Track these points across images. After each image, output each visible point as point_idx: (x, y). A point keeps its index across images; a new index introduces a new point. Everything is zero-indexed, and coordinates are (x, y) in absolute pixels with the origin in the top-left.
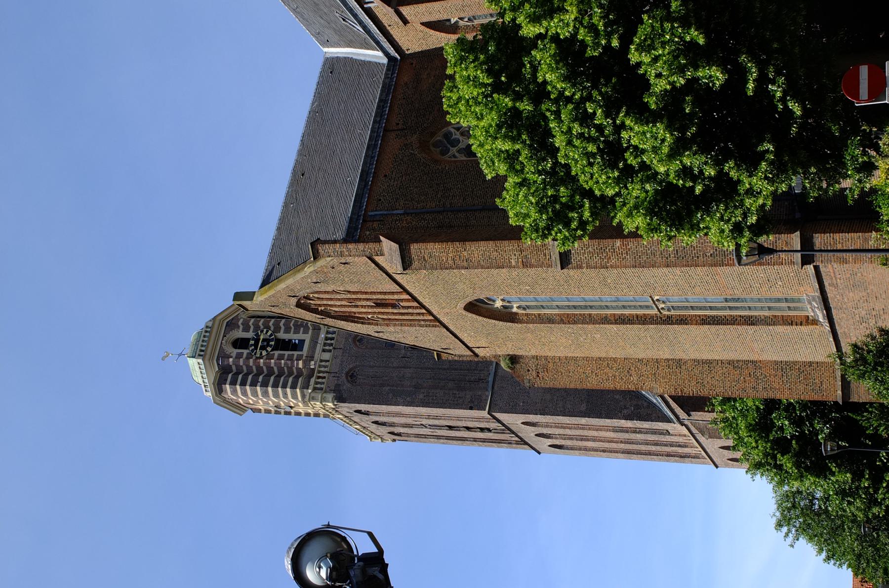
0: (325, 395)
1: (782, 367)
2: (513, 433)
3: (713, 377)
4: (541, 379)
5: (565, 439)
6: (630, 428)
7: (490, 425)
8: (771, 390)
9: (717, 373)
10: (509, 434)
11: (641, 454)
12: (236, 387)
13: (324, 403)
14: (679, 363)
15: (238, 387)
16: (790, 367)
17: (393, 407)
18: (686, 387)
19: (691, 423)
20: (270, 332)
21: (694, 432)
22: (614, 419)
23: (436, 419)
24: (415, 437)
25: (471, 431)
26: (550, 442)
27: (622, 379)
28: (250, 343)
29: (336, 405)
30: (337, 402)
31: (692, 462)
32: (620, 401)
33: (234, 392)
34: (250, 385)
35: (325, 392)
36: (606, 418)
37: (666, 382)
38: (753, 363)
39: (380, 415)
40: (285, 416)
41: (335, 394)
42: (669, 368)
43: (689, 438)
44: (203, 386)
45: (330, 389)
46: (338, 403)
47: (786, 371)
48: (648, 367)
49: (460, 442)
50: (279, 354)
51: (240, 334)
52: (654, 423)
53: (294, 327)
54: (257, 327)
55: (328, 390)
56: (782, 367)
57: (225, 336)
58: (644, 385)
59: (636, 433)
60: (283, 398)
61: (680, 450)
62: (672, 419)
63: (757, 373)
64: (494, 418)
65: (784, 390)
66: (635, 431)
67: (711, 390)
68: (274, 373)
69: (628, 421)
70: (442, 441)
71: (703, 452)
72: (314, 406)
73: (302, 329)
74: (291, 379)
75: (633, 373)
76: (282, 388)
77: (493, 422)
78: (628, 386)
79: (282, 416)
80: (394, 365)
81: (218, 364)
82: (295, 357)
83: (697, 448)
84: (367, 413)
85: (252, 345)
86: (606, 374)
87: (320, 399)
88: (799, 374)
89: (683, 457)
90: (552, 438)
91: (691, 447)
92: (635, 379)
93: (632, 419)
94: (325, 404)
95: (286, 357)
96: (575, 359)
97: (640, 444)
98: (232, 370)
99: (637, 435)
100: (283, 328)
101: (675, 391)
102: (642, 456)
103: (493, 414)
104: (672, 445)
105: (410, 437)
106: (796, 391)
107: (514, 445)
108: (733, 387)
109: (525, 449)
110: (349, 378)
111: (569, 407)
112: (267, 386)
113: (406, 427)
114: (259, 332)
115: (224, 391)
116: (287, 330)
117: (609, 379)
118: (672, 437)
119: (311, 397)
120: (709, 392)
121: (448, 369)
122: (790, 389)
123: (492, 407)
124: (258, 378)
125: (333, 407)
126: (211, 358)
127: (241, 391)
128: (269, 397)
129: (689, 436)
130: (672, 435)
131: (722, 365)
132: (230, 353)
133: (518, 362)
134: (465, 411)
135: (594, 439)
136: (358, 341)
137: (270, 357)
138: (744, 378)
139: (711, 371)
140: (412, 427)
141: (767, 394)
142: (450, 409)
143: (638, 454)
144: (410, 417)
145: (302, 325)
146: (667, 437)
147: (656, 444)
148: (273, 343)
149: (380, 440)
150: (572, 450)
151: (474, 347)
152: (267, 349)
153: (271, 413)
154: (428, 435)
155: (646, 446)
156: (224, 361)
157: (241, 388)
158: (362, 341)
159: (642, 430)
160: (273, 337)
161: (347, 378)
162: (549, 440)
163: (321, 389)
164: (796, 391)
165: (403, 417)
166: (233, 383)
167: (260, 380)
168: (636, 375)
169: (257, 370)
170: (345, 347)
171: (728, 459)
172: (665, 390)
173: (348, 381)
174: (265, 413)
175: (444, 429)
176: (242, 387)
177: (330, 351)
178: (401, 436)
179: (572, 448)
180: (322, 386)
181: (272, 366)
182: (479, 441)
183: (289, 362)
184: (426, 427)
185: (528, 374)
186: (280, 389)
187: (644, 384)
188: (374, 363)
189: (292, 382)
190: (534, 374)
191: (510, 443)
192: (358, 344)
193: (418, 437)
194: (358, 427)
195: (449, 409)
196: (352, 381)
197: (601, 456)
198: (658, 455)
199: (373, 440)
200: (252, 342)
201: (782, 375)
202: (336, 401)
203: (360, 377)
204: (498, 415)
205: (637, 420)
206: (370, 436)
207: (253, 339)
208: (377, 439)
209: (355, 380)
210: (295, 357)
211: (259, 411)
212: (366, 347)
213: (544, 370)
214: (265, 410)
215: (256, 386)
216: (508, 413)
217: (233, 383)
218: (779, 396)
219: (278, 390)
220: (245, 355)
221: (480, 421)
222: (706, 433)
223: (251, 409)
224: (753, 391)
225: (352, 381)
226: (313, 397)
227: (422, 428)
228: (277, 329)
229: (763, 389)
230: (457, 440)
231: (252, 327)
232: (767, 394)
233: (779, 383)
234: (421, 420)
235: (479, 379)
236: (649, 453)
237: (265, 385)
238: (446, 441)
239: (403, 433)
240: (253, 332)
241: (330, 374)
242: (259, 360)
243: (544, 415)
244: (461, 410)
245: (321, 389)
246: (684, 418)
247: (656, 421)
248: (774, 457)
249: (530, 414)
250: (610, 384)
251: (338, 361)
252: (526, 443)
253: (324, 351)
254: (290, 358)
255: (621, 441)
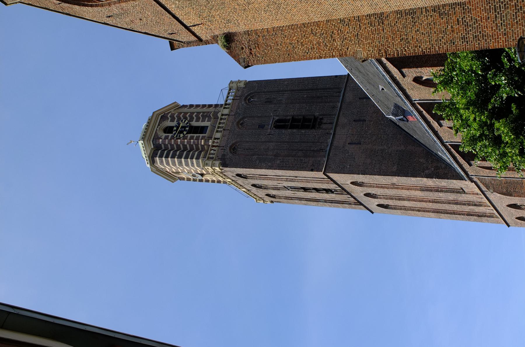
0: (214, 162)
1: (495, 5)
2: (348, 193)
3: (418, 31)
4: (254, 56)
5: (387, 199)
6: (433, 188)
7: (330, 186)
8: (483, 39)
9: (421, 24)
10: (346, 194)
11: (448, 214)
12: (162, 159)
13: (213, 168)
14: (381, 17)
15: (164, 159)
16: (505, 5)
17: (259, 170)
18: (389, 47)
19: (479, 179)
20: (187, 121)
21: (484, 190)
22: (418, 177)
23: (292, 181)
24: (285, 199)
25: (320, 193)
26: (376, 201)
27: (326, 46)
28: (174, 129)
29: (222, 169)
30: (222, 167)
31: (488, 221)
32: (424, 164)
33: (162, 162)
34: (171, 158)
35: (215, 160)
36: (412, 177)
37: (369, 43)
38: (461, 6)
39: (254, 179)
40: (200, 182)
41: (221, 161)
42: (371, 25)
43: (481, 196)
44: (146, 160)
45: (218, 158)
46: (223, 168)
47: (500, 10)
48: (351, 27)
49: (315, 203)
50: (191, 136)
51: (168, 123)
52: (450, 180)
53: (202, 117)
54: (179, 118)
55: (217, 158)
56: (495, 5)
57: (159, 125)
58: (347, 50)
59: (438, 192)
60: (192, 166)
61: (477, 209)
62: (463, 176)
63: (467, 18)
64: (329, 177)
65: (498, 35)
66: (438, 190)
67: (416, 47)
68: (188, 150)
69: (429, 179)
70: (303, 202)
71: (495, 212)
72: (208, 170)
73: (207, 118)
74: (196, 153)
75: (336, 36)
76: (190, 159)
77: (331, 183)
78: (332, 52)
79: (198, 182)
80: (262, 140)
81: (153, 144)
82: (200, 138)
83: (490, 207)
84: (245, 177)
85: (175, 130)
86: (311, 42)
87: (211, 164)
88: (516, 13)
89: (481, 216)
90: (377, 198)
91: (485, 206)
92: (338, 44)
93: (432, 177)
94: (214, 169)
95: (195, 138)
96: (281, 29)
97: (444, 203)
98: (162, 148)
99: (440, 194)
100: (195, 118)
101: (379, 53)
102: (449, 215)
103: (328, 174)
104: (469, 204)
105: (281, 199)
106: (513, 36)
107: (353, 206)
108: (440, 41)
109: (360, 209)
110: (232, 150)
111: (384, 168)
112: (181, 158)
113: (275, 189)
114: (180, 121)
115: (155, 162)
116: (197, 120)
117: (314, 48)
118: (467, 196)
119: (205, 163)
120: (415, 50)
121: (298, 142)
122: (505, 33)
123: (327, 169)
124: (177, 153)
125: (220, 171)
126: (149, 140)
127: (166, 161)
128: (183, 166)
129: (480, 195)
130: (467, 194)
131: (426, 13)
132: (161, 136)
133: (233, 40)
134: (308, 172)
135: (409, 199)
136: (240, 124)
137: (185, 138)
138: (452, 27)
139: (415, 23)
140: (279, 190)
141: (479, 44)
142: (297, 171)
143: (445, 213)
144: (274, 180)
145: (206, 116)
146: (463, 195)
147: (457, 203)
148: (187, 129)
149: (262, 202)
150: (395, 209)
151: (191, 26)
152: (184, 133)
153: (190, 181)
154: (293, 198)
155: (449, 205)
156: (157, 142)
157: (165, 160)
158: (243, 124)
159: (443, 189)
160: (188, 124)
161: (230, 150)
162: (376, 200)
163: (212, 158)
164: (513, 36)
165: (270, 180)
166: (161, 156)
167: (178, 154)
168: (339, 39)
169: (177, 148)
170: (231, 129)
171: (517, 218)
172: (369, 53)
173: (231, 152)
174: (187, 180)
175: (301, 191)
176: (166, 159)
177: (221, 132)
178: (275, 198)
179: (395, 208)
180: (214, 156)
181: (185, 144)
182: (328, 202)
183: (196, 141)
184: (289, 189)
185: (242, 52)
186: (189, 160)
187: (347, 49)
188: (249, 139)
189: (197, 155)
190: (248, 51)
191: (350, 204)
192: (240, 126)
193: (287, 199)
194: (244, 190)
195: (296, 171)
196: (233, 152)
197: (417, 216)
198: (460, 215)
199: (258, 201)
200: (175, 128)
201: (496, 17)
202: (221, 166)
203: (239, 149)
204: (331, 175)
205: (435, 178)
206: (256, 199)
207: (176, 126)
208: (261, 201)
209: (235, 152)
210: (200, 138)
211: (183, 179)
212: (245, 128)
213: (256, 46)
214: (187, 178)
215: (174, 158)
216: (338, 173)
217: (161, 156)
218: (493, 44)
219: (188, 161)
220: (170, 138)
221: (322, 183)
222: (491, 187)
223: (179, 178)
224: (463, 43)
225: (233, 152)
226: (207, 163)
227: (286, 190)
228: (192, 119)
229: (473, 38)
230: (313, 201)
231: (176, 119)
232: (479, 44)
233: (492, 27)
234: (282, 182)
235: (320, 149)
236: (454, 213)
237: (180, 157)
238: (306, 202)
239: (277, 196)
240: (176, 122)
241: (219, 147)
242: (177, 140)
243: (364, 174)
244: (305, 172)
245: (212, 158)
246: (472, 174)
247: (451, 179)
248: (491, 127)
249: (354, 174)
250: (316, 53)
251: (226, 138)
252: (361, 204)
253: (217, 131)
254: (198, 138)
255: (430, 201)
